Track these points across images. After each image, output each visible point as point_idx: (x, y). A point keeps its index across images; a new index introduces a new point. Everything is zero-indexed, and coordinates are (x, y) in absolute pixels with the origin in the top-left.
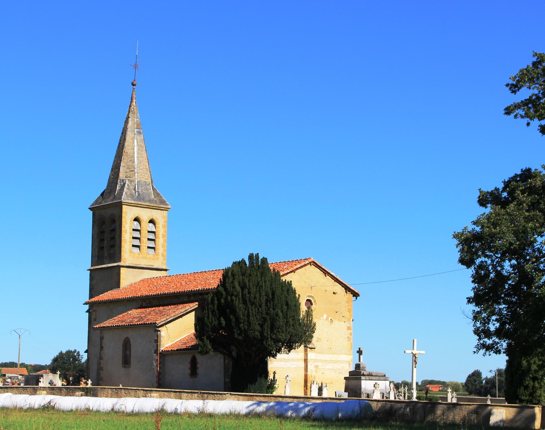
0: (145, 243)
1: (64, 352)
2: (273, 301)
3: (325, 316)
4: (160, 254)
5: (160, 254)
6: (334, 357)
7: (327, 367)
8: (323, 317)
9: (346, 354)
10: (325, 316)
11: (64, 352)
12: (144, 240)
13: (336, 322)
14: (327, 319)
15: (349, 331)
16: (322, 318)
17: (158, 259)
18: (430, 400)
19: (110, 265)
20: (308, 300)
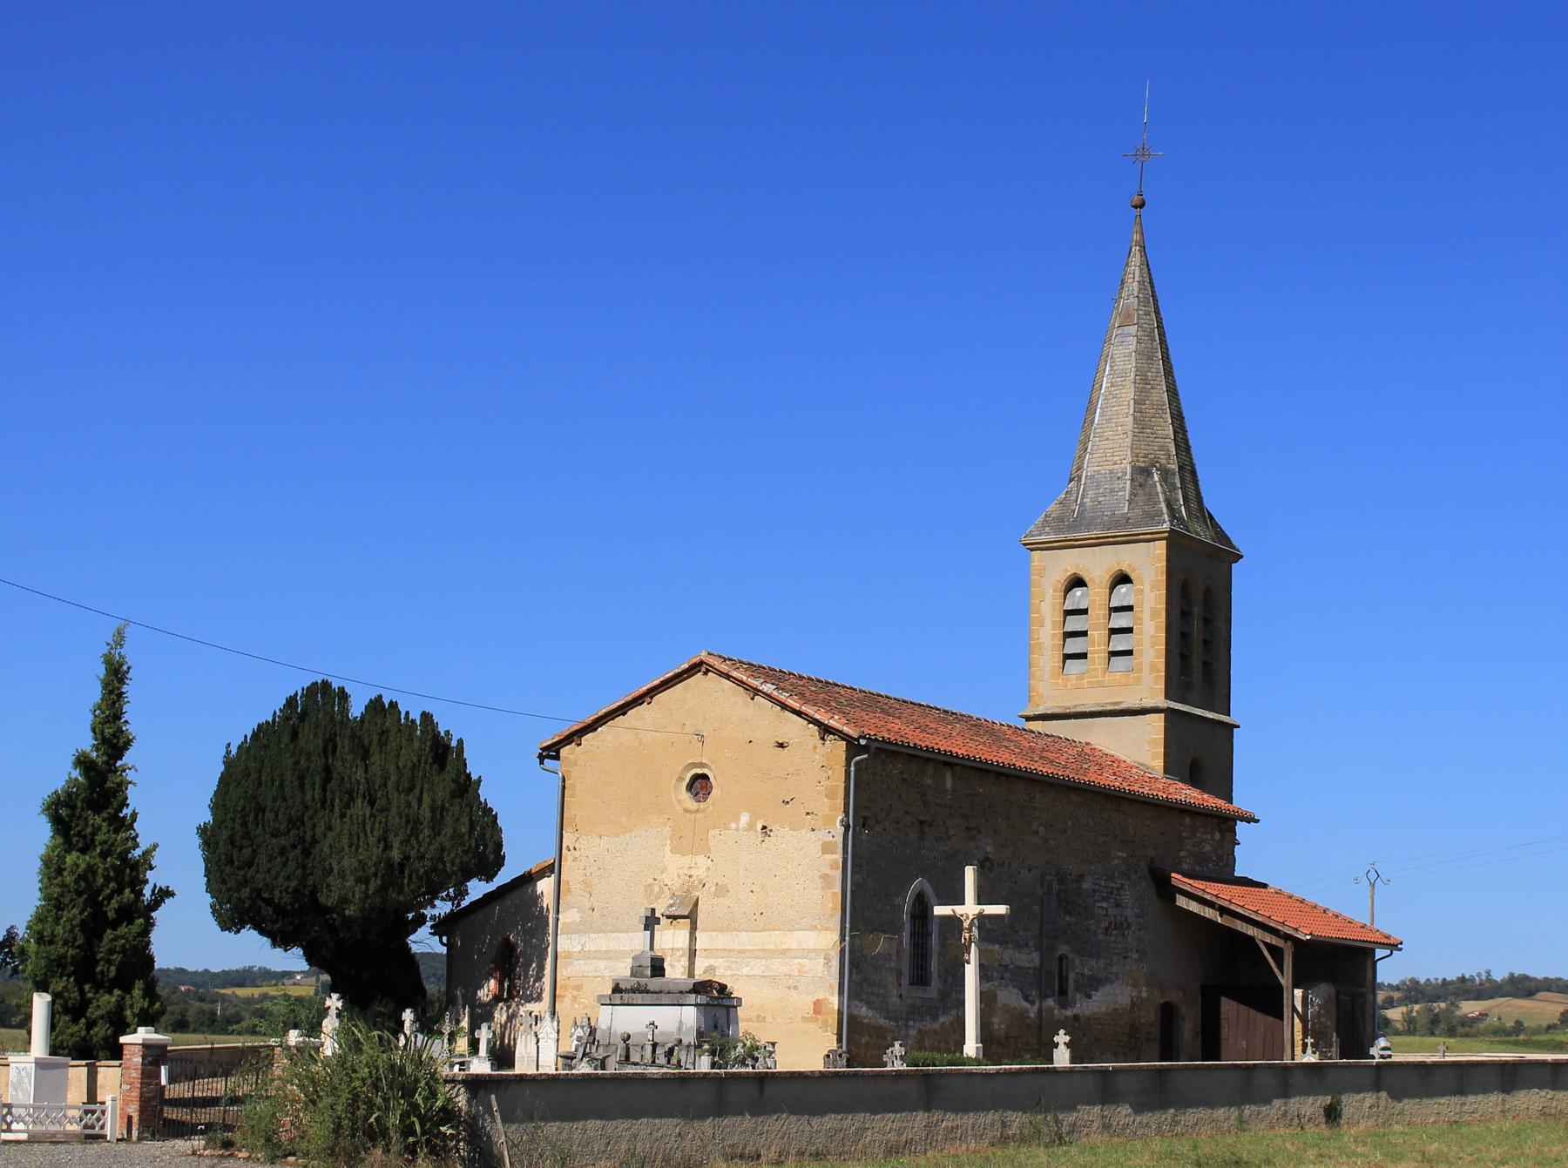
0: (1096, 644)
1: (207, 817)
2: (303, 802)
3: (745, 819)
4: (1146, 669)
5: (1146, 669)
6: (774, 939)
7: (746, 970)
8: (737, 820)
9: (814, 928)
10: (745, 819)
11: (207, 817)
12: (1098, 635)
13: (779, 832)
14: (751, 826)
15: (828, 857)
16: (733, 826)
17: (1138, 681)
18: (700, 1034)
19: (1199, 712)
20: (690, 787)
